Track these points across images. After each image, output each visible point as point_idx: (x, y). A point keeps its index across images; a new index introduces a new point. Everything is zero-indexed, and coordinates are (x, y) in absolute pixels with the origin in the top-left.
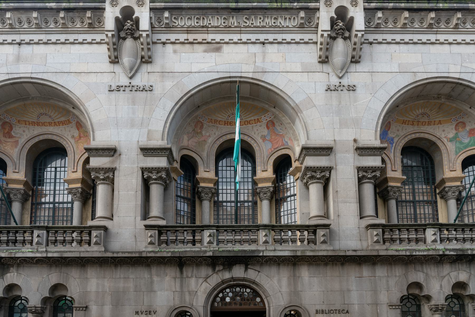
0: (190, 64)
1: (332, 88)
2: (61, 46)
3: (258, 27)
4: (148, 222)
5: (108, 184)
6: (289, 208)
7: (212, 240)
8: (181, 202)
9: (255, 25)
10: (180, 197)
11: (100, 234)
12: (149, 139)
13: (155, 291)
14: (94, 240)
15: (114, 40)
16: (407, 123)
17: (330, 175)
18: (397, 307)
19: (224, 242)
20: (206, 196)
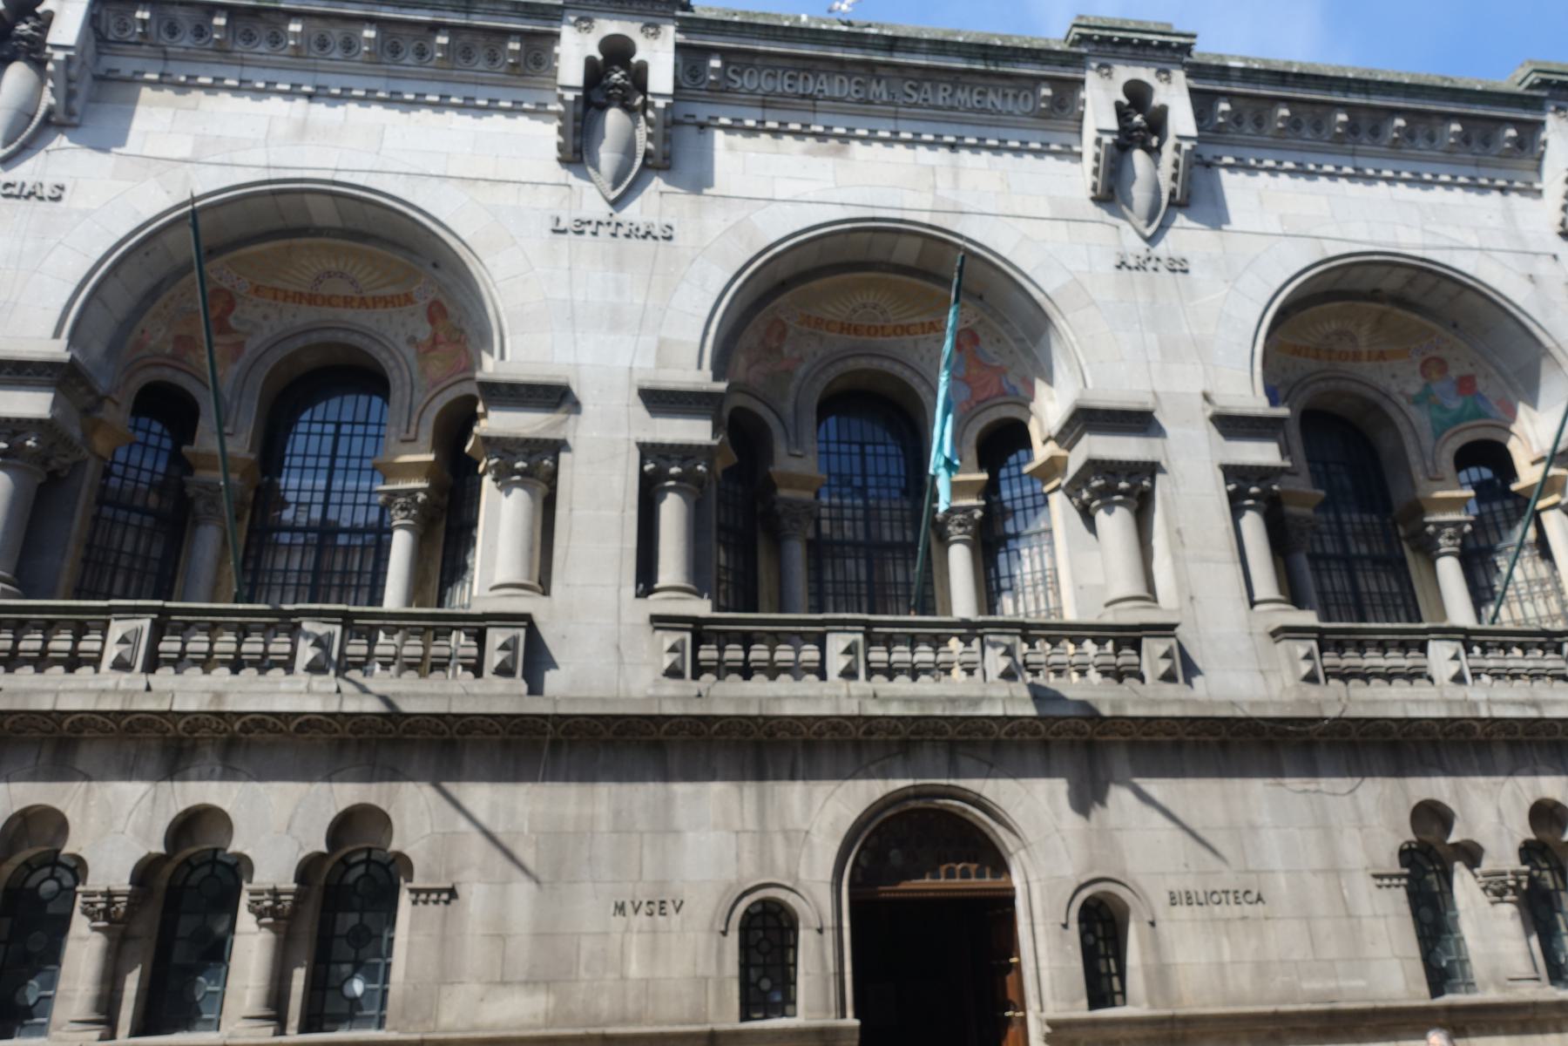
0: (780, 185)
1: (1132, 262)
4: (659, 604)
9: (931, 101)
11: (683, 642)
12: (661, 362)
13: (677, 832)
14: (494, 658)
18: (1395, 881)
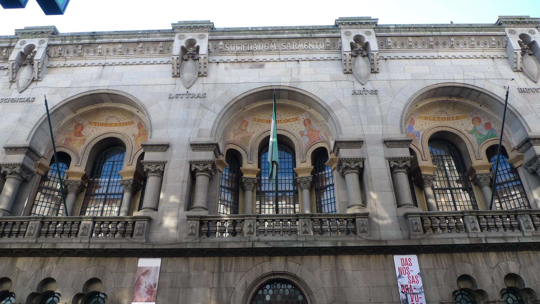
2: (68, 68)
3: (292, 50)
4: (191, 213)
5: (158, 176)
6: (329, 198)
7: (252, 231)
8: (225, 192)
10: (225, 187)
11: (144, 224)
12: (199, 136)
15: (178, 62)
16: (428, 118)
17: (164, 169)
19: (280, 232)
20: (249, 186)
